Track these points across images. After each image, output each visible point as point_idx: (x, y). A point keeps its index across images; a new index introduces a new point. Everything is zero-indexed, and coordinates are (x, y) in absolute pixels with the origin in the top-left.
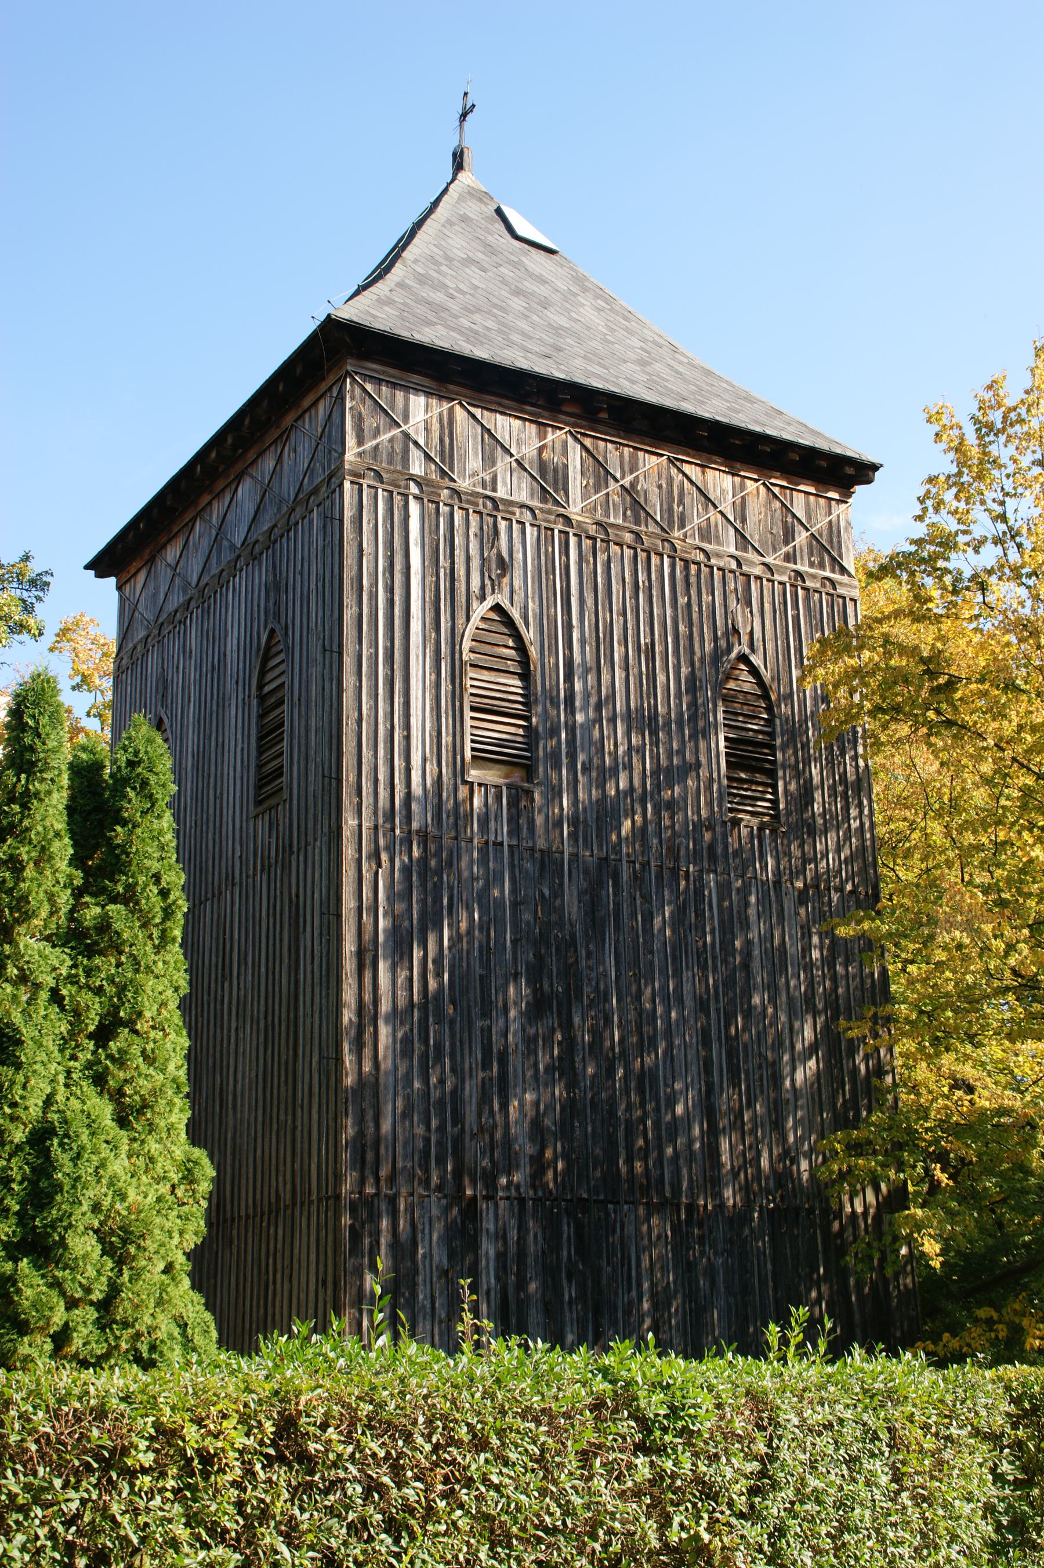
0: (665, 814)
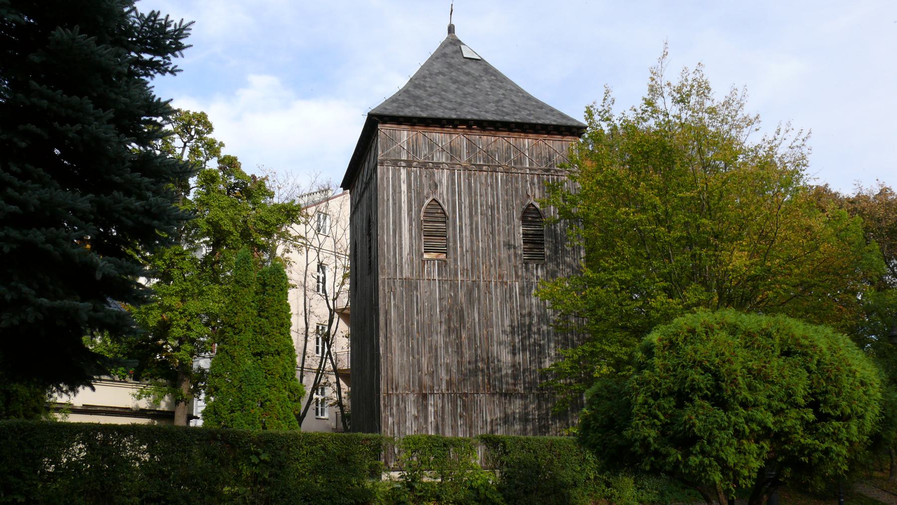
0: (445, 104)
